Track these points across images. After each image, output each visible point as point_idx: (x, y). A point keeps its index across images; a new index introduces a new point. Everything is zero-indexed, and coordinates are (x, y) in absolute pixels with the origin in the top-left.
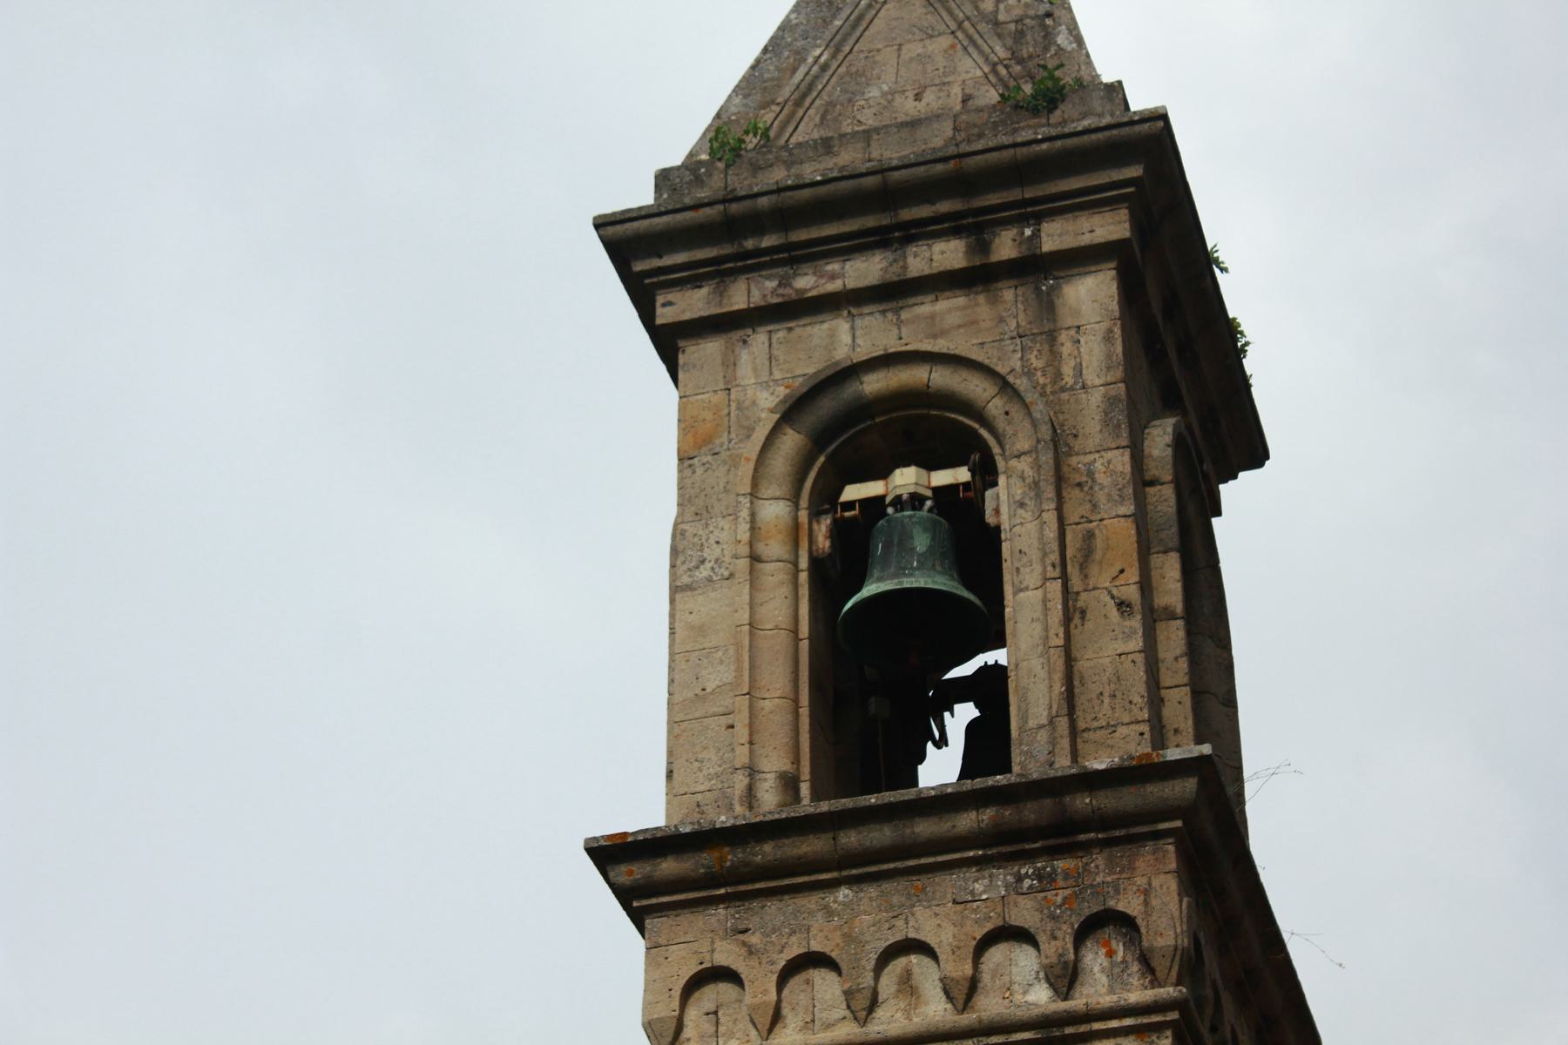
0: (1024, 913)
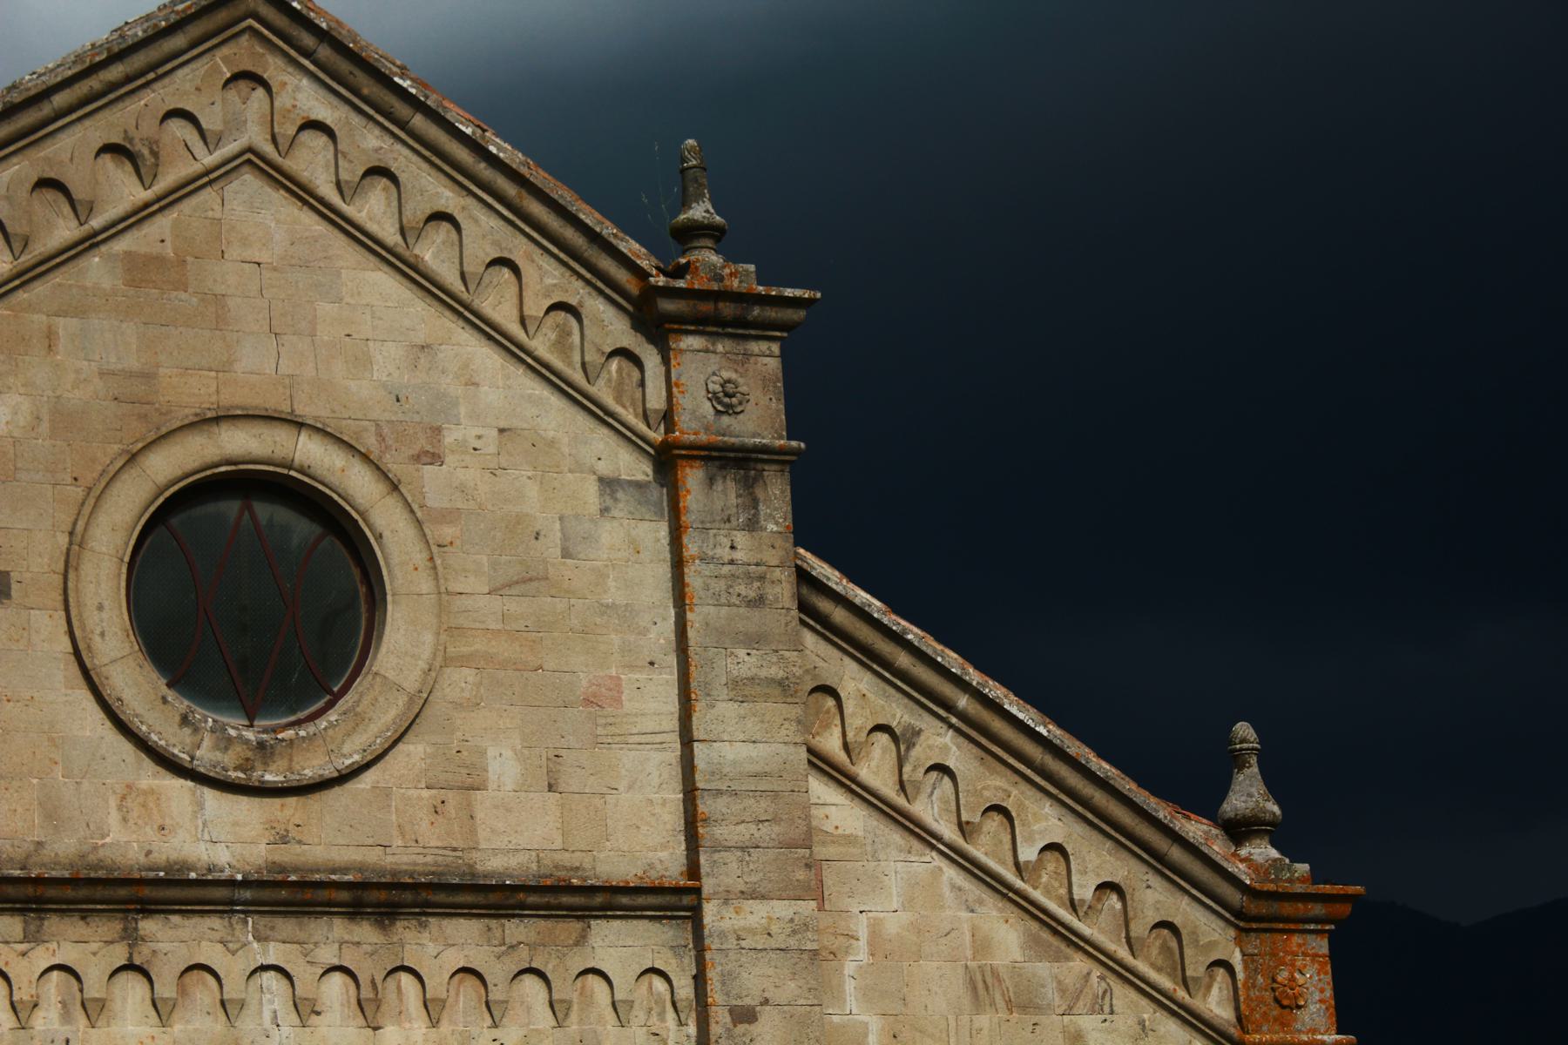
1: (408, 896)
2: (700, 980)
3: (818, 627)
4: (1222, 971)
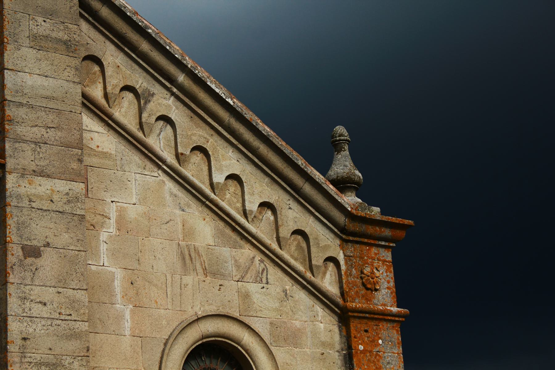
3: (90, 19)
4: (332, 264)
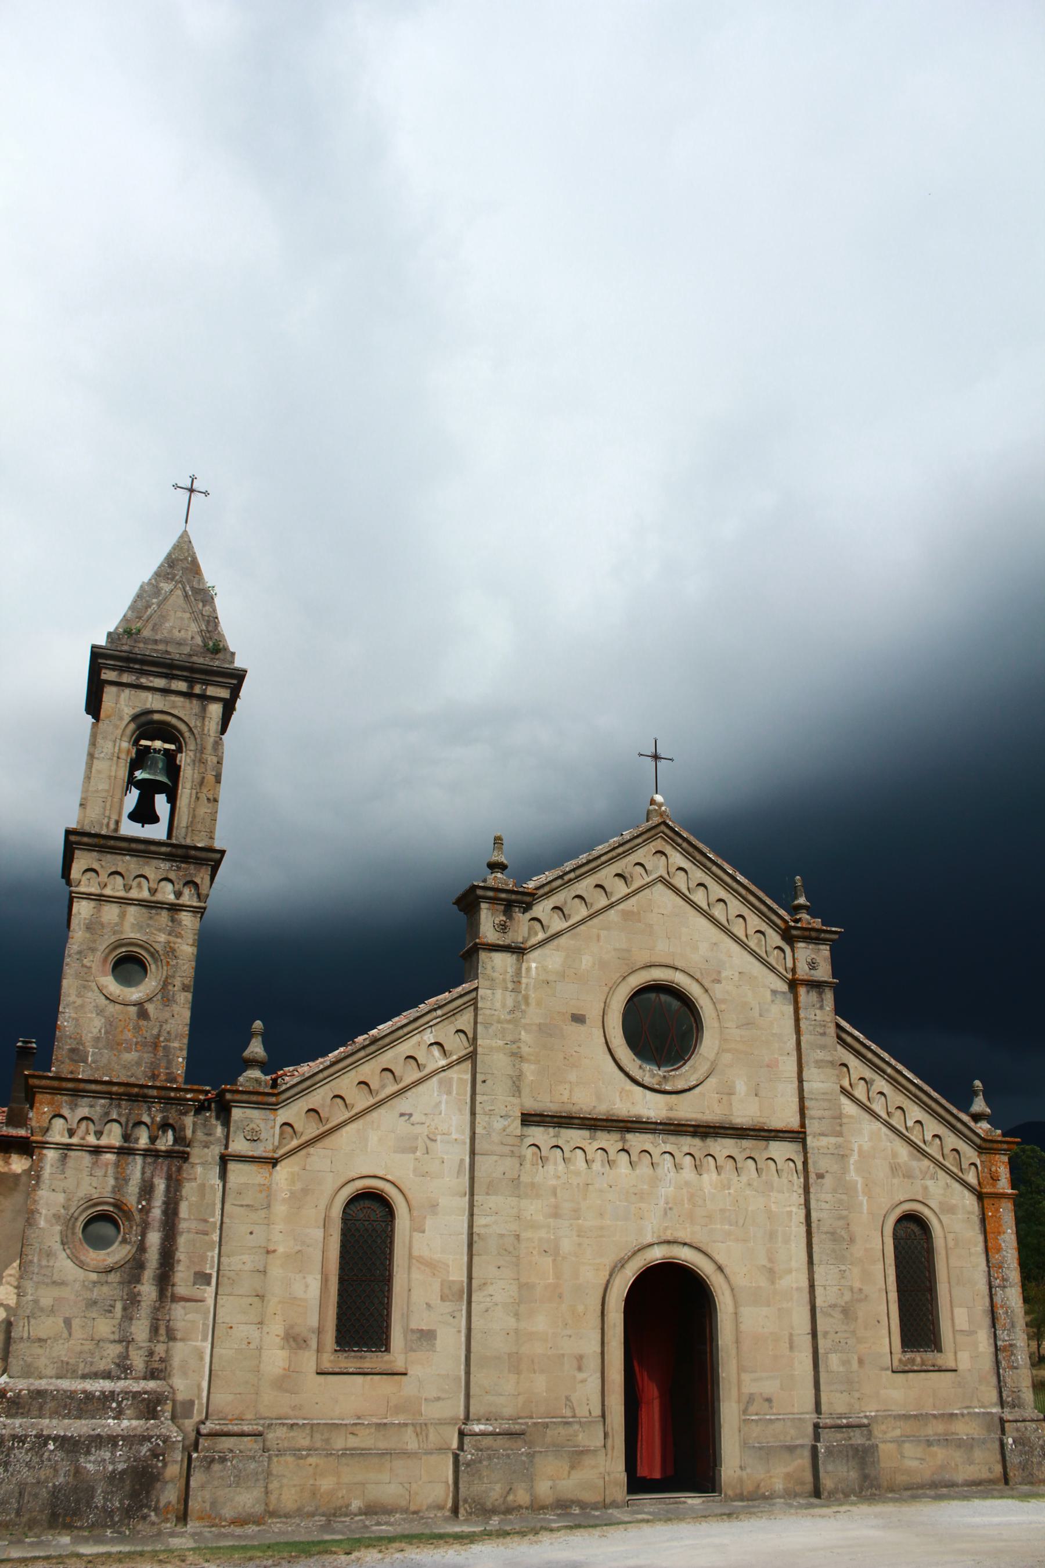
0: (172, 875)
1: (712, 1130)
2: (805, 1163)
